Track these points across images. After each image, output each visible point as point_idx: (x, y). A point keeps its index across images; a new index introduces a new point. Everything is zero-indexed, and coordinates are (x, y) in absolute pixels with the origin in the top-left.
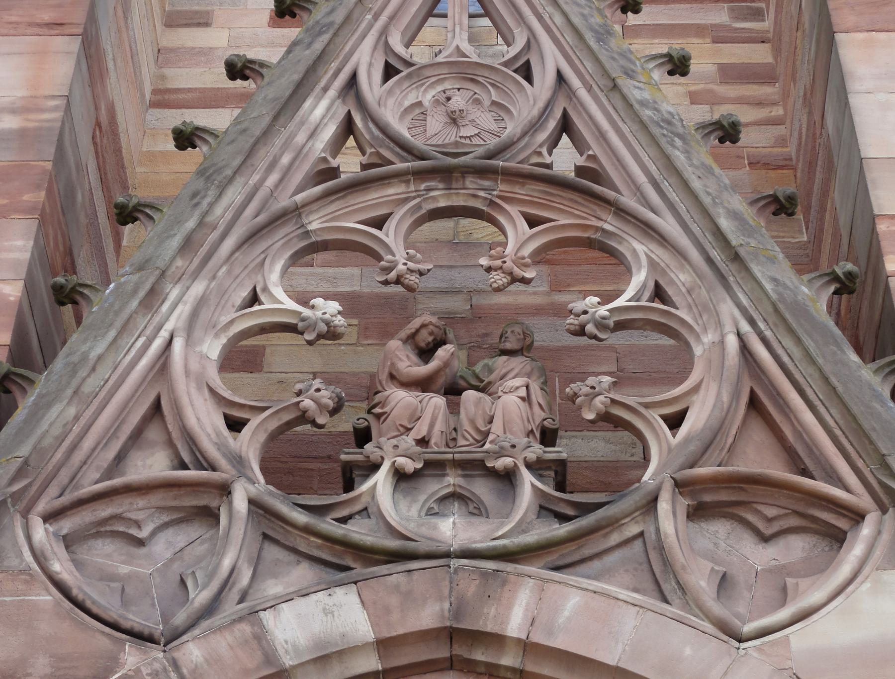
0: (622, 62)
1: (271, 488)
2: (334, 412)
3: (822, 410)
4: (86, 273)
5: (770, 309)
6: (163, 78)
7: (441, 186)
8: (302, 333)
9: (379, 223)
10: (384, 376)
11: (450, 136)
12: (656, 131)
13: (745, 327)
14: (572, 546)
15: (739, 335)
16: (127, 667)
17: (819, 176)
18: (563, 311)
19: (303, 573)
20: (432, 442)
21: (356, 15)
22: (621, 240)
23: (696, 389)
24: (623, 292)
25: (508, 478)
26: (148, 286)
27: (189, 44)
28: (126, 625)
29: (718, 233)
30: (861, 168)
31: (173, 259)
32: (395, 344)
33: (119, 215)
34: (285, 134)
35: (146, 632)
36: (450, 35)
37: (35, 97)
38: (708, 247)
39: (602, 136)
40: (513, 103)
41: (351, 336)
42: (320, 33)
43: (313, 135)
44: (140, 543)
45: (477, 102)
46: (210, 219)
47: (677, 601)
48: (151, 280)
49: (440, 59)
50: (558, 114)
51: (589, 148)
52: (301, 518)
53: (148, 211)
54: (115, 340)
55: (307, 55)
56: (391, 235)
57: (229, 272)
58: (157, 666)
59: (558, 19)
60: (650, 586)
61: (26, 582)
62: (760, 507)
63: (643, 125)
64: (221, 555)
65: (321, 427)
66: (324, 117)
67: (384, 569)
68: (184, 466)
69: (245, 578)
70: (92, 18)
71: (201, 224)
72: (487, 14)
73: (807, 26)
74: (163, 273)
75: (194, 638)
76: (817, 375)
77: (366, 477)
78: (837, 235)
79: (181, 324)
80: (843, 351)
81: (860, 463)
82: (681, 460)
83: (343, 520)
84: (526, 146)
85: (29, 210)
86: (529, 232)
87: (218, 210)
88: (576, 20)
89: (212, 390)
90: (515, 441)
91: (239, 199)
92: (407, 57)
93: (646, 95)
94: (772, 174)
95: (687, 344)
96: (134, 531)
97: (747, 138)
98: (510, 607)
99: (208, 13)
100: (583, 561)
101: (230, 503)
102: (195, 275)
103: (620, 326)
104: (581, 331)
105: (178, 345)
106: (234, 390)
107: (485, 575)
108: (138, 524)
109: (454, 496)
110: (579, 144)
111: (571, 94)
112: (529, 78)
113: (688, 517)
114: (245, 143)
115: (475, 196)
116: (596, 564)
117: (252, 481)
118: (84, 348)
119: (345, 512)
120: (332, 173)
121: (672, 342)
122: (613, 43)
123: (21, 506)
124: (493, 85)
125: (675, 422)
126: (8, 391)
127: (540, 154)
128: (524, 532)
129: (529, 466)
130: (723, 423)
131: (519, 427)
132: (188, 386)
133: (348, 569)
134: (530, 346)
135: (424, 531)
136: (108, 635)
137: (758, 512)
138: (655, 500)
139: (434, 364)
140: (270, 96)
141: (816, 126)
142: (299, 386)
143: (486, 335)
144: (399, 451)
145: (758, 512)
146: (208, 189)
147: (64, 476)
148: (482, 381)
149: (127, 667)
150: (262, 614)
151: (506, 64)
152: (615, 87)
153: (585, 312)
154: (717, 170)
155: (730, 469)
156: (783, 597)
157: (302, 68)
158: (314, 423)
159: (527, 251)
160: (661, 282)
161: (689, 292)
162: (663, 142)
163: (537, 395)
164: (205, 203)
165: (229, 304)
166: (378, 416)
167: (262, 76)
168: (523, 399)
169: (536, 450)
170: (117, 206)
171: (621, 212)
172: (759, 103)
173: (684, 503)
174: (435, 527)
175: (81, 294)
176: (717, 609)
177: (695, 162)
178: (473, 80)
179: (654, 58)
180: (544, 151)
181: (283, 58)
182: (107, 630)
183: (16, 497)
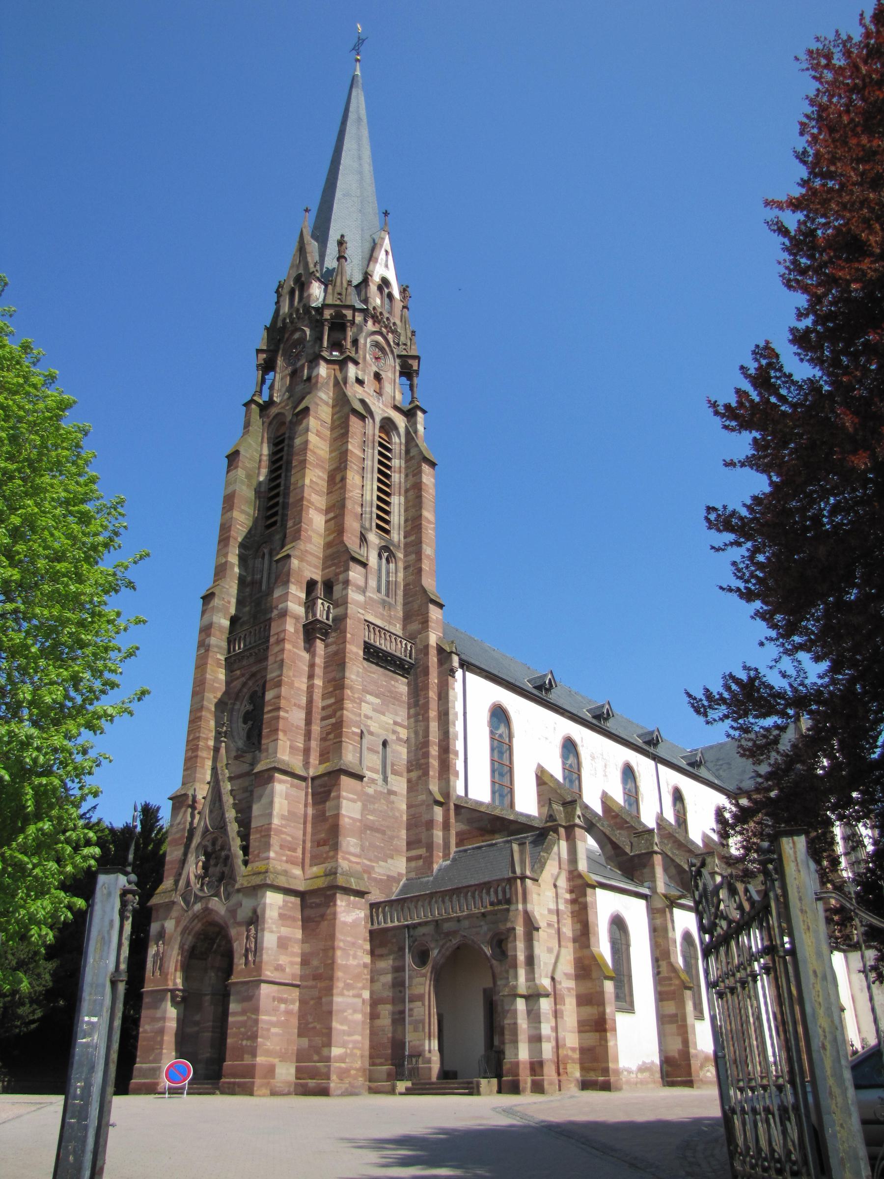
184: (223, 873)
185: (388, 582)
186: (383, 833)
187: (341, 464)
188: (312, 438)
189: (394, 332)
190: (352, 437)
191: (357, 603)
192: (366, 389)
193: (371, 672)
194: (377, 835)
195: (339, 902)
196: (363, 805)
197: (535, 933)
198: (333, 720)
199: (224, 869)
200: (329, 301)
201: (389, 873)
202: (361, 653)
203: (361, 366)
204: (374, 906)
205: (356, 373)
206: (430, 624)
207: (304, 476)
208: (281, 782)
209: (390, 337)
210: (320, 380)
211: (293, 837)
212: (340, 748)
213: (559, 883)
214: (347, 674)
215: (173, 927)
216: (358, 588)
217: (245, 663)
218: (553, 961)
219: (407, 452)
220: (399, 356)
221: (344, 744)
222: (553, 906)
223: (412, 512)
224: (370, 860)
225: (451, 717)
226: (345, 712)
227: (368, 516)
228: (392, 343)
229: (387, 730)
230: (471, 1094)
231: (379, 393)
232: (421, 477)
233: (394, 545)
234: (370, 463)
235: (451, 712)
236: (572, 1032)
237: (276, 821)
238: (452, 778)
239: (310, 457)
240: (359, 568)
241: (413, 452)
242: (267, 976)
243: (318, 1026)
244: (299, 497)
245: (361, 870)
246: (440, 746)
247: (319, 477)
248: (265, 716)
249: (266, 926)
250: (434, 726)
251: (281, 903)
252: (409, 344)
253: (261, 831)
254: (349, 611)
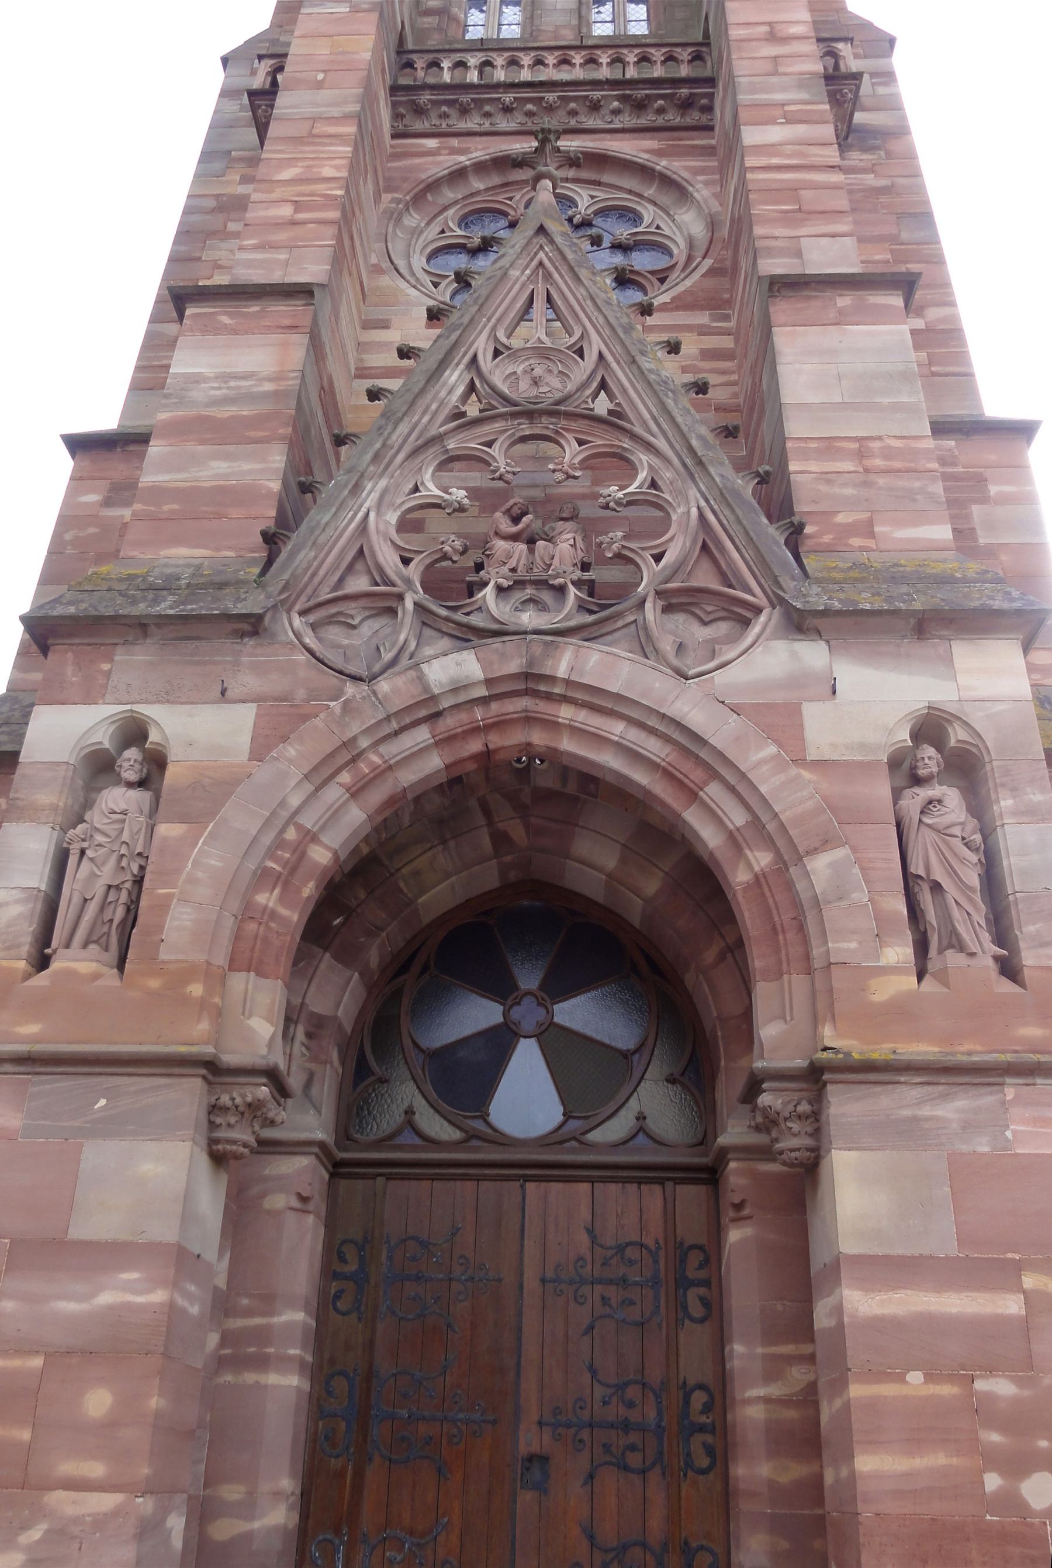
0: (639, 346)
1: (427, 596)
2: (462, 553)
3: (744, 551)
4: (319, 476)
5: (718, 493)
6: (362, 360)
7: (527, 422)
8: (444, 509)
9: (489, 444)
10: (492, 533)
11: (534, 392)
12: (657, 387)
13: (703, 503)
14: (596, 627)
15: (698, 508)
16: (348, 695)
17: (755, 415)
18: (597, 496)
19: (445, 643)
20: (519, 570)
21: (476, 318)
22: (632, 453)
23: (671, 539)
24: (631, 485)
25: (561, 590)
26: (353, 482)
27: (377, 339)
28: (347, 672)
29: (691, 450)
30: (781, 409)
31: (368, 466)
32: (498, 515)
33: (335, 441)
34: (433, 391)
35: (358, 675)
36: (534, 331)
37: (283, 371)
38: (684, 457)
39: (624, 391)
40: (571, 371)
41: (474, 511)
42: (455, 330)
43: (450, 392)
44: (354, 627)
45: (550, 371)
46: (389, 442)
47: (653, 658)
48: (355, 478)
49: (528, 345)
50: (599, 378)
51: (617, 399)
52: (443, 612)
53: (353, 438)
54: (335, 513)
55: (447, 343)
56: (496, 451)
57: (401, 473)
58: (364, 694)
59: (601, 320)
60: (638, 649)
61: (291, 649)
62: (704, 606)
63: (649, 384)
64: (399, 633)
65: (454, 562)
66: (456, 382)
67: (490, 640)
68: (377, 584)
69: (413, 645)
70: (315, 323)
71: (384, 445)
72: (559, 319)
73: (756, 324)
74: (362, 475)
75: (385, 679)
76: (742, 531)
77: (481, 590)
78: (763, 452)
79: (373, 504)
80: (758, 517)
81: (763, 581)
82: (660, 579)
83: (468, 614)
84: (578, 398)
85: (282, 438)
86: (579, 449)
87: (394, 437)
88: (612, 320)
89: (392, 542)
90: (565, 569)
91: (406, 430)
92: (508, 344)
93: (653, 366)
94: (728, 415)
95: (668, 514)
96: (349, 621)
97: (711, 393)
98: (559, 661)
99: (388, 320)
100: (602, 636)
101: (404, 605)
102: (381, 476)
103: (630, 503)
104: (606, 507)
105: (372, 516)
106: (407, 543)
107: (546, 643)
108: (352, 617)
109: (531, 600)
110: (611, 396)
111: (607, 366)
112: (582, 357)
113: (663, 611)
114: (409, 397)
115: (548, 428)
116: (609, 638)
117: (416, 592)
118: (318, 518)
119: (468, 610)
120: (463, 414)
121: (662, 514)
122: (634, 334)
123: (286, 607)
124: (559, 361)
125: (658, 558)
126: (276, 543)
127: (587, 402)
128: (569, 620)
129: (573, 583)
130: (685, 560)
131: (568, 561)
132: (378, 539)
133: (471, 641)
134: (577, 516)
135: (513, 620)
136: (337, 677)
137: (702, 609)
138: (644, 601)
139: (520, 526)
140: (424, 369)
141: (756, 385)
142: (442, 539)
143: (553, 511)
144: (499, 575)
145: (702, 609)
146: (387, 424)
147: (309, 590)
148: (548, 536)
149: (348, 695)
150: (422, 665)
151: (568, 348)
152: (634, 361)
153: (610, 496)
154: (693, 411)
155: (687, 584)
156: (713, 655)
157: (443, 351)
158: (451, 559)
159: (577, 460)
160: (656, 478)
161: (671, 483)
162: (661, 395)
163: (580, 544)
164: (386, 433)
165: (402, 493)
166: (488, 556)
167: (419, 356)
168: (571, 545)
169: (578, 574)
170: (334, 435)
171: (634, 437)
172: (723, 372)
173: (660, 603)
174: (519, 618)
175: (316, 487)
176: (675, 662)
177: (680, 406)
178: (547, 358)
179: (659, 343)
180: (590, 400)
181: (432, 346)
182: (337, 674)
183: (283, 602)
215: (244, 741)
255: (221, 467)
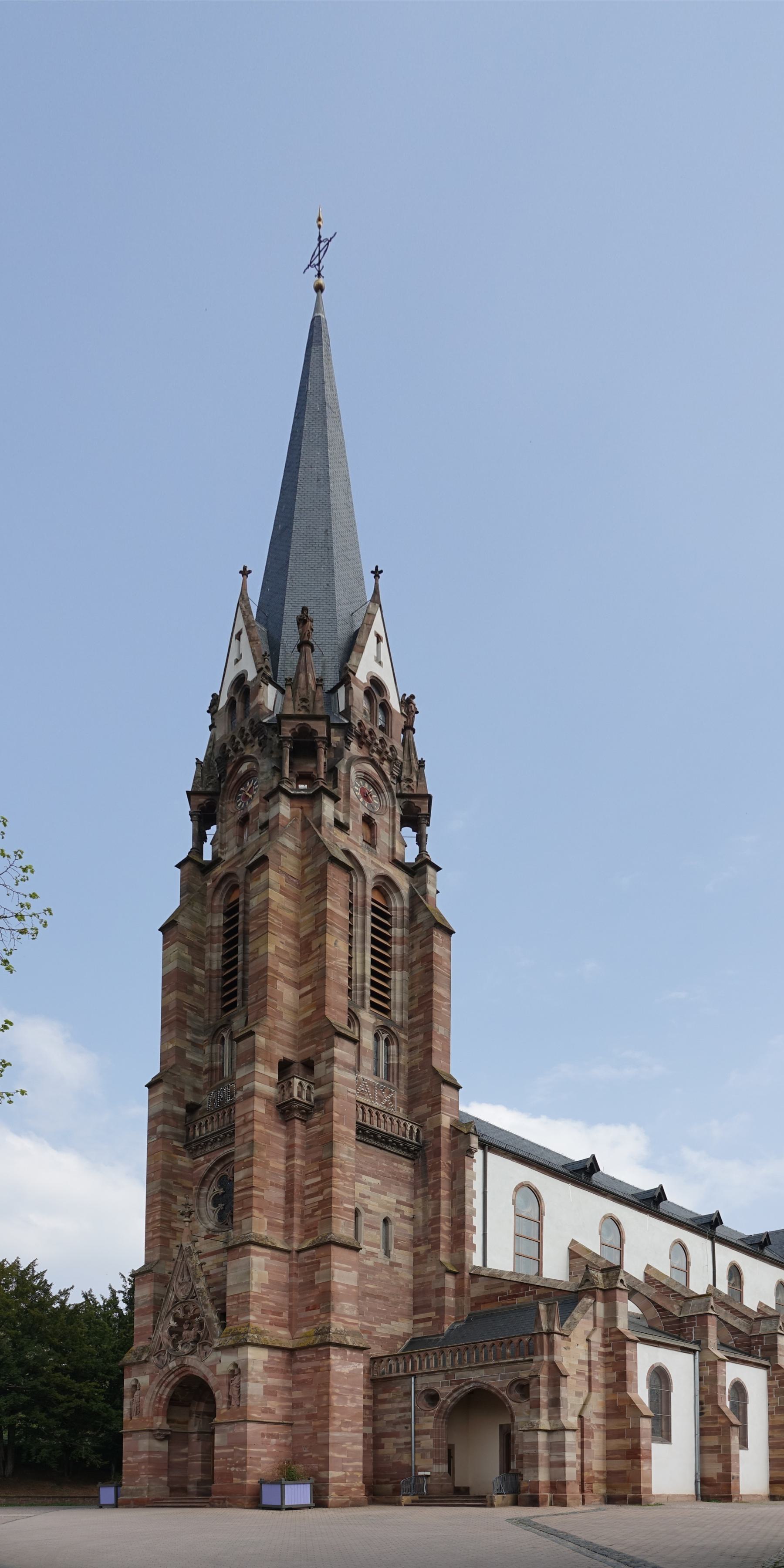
184: (198, 1335)
185: (388, 1066)
186: (386, 1299)
187: (317, 927)
188: (275, 896)
189: (392, 761)
190: (332, 894)
191: (346, 1082)
192: (351, 837)
193: (367, 1154)
194: (378, 1301)
195: (332, 1357)
196: (360, 1275)
197: (562, 1379)
198: (320, 1198)
199: (199, 1332)
200: (289, 711)
201: (393, 1333)
202: (354, 1133)
203: (341, 802)
204: (374, 1360)
205: (335, 814)
206: (442, 1105)
207: (266, 943)
208: (258, 1254)
209: (385, 766)
210: (281, 822)
211: (276, 1303)
212: (330, 1223)
213: (592, 1339)
214: (335, 1153)
215: (148, 1382)
216: (347, 1066)
217: (209, 1149)
218: (582, 1403)
219: (412, 917)
220: (400, 796)
221: (334, 1219)
222: (584, 1358)
223: (419, 990)
224: (370, 1322)
225: (467, 1196)
226: (334, 1189)
227: (359, 992)
228: (389, 777)
229: (388, 1208)
230: (485, 1506)
231: (371, 843)
232: (432, 947)
233: (396, 1026)
234: (359, 931)
235: (467, 1190)
236: (599, 1459)
237: (255, 1289)
238: (467, 1250)
239: (273, 919)
240: (348, 1044)
241: (421, 918)
242: (254, 1417)
243: (314, 1456)
244: (263, 967)
245: (358, 1330)
246: (452, 1221)
247: (288, 944)
248: (235, 1196)
249: (249, 1377)
250: (445, 1204)
251: (266, 1358)
252: (415, 779)
253: (238, 1299)
254: (335, 1090)
255: (144, 1321)
